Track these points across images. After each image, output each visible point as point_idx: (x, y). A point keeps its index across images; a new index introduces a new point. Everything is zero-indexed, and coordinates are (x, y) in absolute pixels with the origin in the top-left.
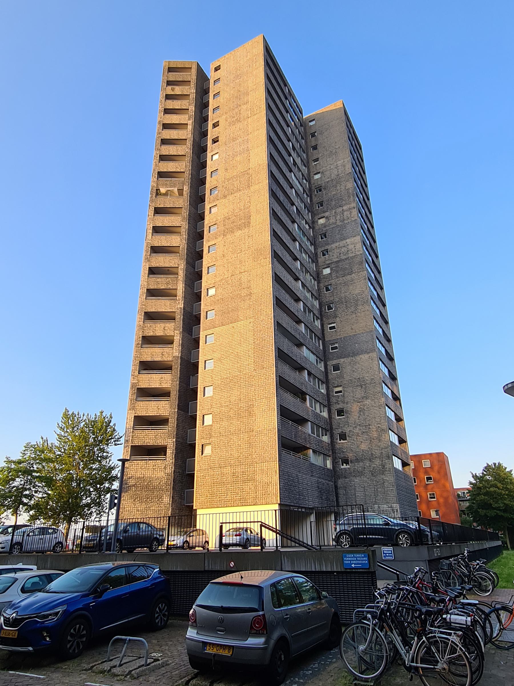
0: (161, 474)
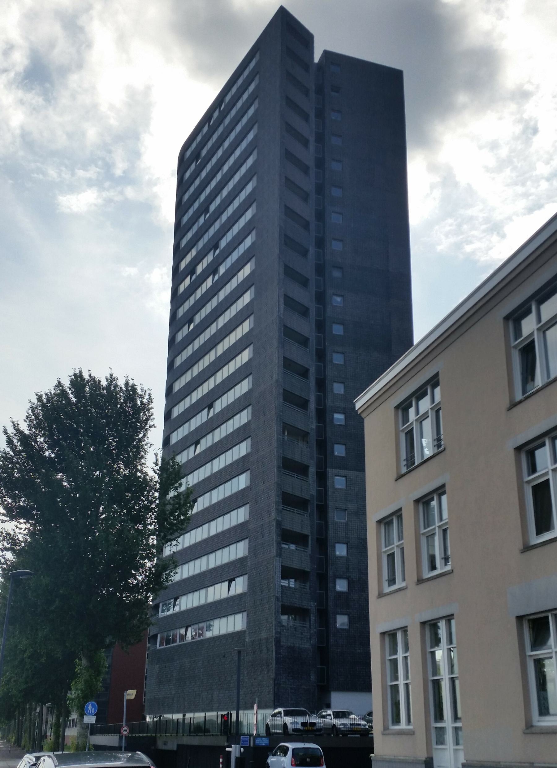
0: (307, 646)
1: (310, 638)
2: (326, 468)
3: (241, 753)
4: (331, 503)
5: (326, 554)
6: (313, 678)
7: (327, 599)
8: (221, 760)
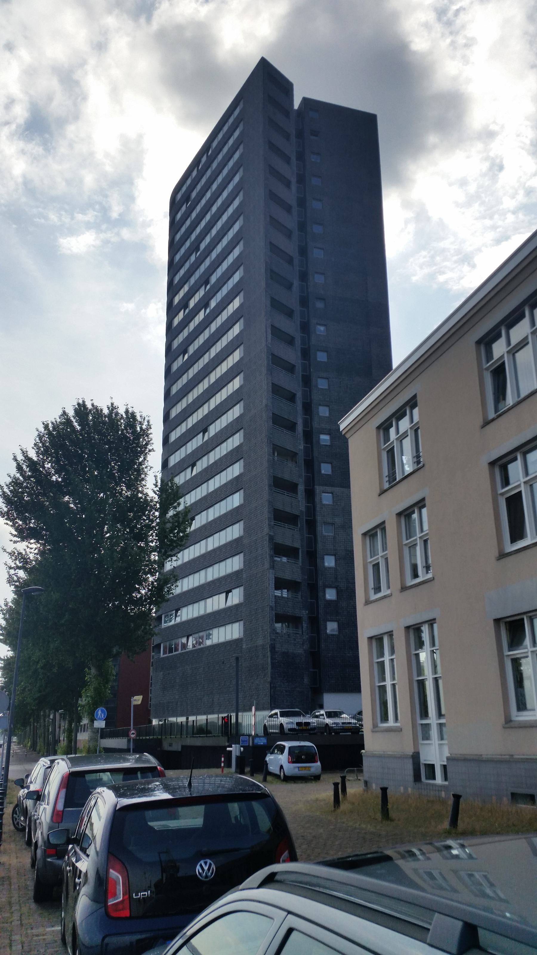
0: (300, 651)
1: (303, 643)
2: (314, 485)
3: (241, 753)
4: (319, 518)
5: (316, 565)
6: (306, 680)
7: (318, 607)
8: (223, 759)
